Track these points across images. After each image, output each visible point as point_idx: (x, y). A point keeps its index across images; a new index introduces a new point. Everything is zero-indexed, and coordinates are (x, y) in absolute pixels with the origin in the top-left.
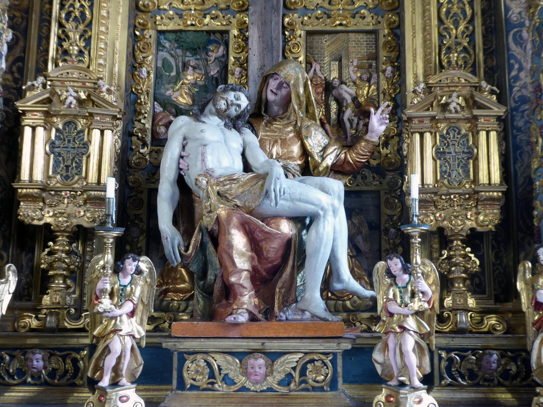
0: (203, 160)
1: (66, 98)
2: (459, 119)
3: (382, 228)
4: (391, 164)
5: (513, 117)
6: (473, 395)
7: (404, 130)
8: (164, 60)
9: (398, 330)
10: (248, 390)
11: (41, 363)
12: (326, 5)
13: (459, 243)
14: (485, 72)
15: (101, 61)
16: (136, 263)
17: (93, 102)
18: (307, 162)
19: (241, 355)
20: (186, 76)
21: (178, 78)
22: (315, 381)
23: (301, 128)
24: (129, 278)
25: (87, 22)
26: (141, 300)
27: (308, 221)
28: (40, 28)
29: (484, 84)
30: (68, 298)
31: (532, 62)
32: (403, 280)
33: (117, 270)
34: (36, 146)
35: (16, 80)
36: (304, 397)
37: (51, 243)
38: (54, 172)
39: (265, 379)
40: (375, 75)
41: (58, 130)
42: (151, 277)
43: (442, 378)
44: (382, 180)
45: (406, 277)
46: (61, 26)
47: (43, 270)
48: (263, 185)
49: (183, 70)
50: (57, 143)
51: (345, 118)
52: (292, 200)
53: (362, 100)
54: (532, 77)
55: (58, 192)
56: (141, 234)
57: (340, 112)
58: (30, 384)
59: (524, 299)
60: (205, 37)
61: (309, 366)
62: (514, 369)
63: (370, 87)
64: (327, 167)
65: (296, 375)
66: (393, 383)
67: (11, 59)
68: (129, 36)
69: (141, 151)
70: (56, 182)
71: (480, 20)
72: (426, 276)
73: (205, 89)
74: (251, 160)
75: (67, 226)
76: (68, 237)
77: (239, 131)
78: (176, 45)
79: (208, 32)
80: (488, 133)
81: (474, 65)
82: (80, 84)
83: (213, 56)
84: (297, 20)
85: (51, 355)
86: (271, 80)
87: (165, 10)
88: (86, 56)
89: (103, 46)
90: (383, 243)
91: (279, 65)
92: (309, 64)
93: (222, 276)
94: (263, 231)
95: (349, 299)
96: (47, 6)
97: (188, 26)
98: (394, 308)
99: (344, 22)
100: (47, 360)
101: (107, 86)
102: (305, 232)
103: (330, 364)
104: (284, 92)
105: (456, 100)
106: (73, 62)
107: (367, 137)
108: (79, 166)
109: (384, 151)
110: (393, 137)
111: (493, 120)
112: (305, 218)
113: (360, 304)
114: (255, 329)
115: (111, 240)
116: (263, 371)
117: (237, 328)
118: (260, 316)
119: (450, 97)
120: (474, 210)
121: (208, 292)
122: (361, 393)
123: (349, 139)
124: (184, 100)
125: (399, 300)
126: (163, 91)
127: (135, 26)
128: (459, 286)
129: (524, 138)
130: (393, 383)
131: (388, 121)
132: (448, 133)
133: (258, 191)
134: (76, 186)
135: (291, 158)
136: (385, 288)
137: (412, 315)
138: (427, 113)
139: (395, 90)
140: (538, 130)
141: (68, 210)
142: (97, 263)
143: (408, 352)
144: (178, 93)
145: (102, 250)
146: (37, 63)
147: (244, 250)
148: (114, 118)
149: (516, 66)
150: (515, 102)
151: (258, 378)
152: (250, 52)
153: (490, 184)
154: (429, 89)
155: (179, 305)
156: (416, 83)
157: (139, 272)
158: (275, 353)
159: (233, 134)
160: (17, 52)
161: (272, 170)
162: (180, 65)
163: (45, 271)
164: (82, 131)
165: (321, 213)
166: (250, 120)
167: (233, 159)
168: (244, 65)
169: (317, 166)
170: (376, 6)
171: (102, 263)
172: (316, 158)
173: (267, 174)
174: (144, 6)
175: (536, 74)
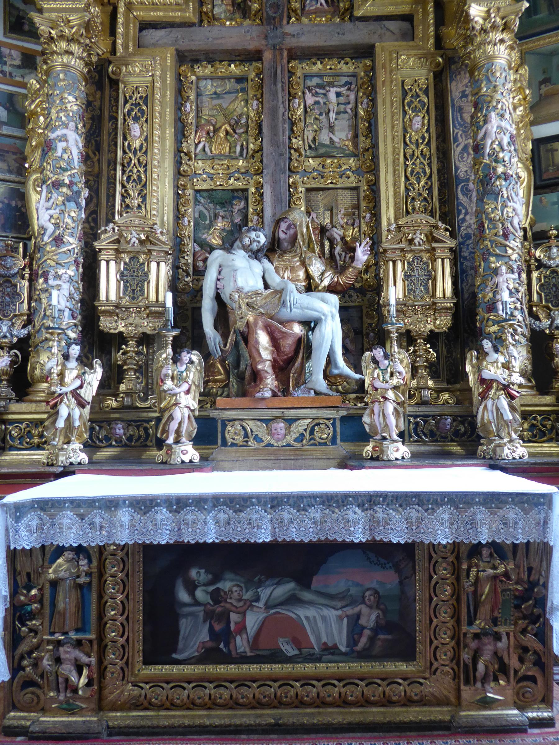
0: (235, 281)
1: (130, 240)
2: (421, 251)
3: (364, 333)
4: (370, 286)
5: (460, 249)
6: (433, 448)
7: (381, 259)
8: (200, 212)
9: (382, 400)
10: (273, 446)
11: (122, 431)
12: (320, 168)
13: (422, 341)
14: (440, 216)
15: (154, 212)
16: (189, 355)
17: (151, 242)
18: (309, 284)
19: (267, 421)
20: (217, 223)
21: (211, 225)
22: (320, 438)
23: (305, 258)
24: (185, 366)
25: (143, 183)
26: (193, 382)
27: (312, 325)
28: (108, 189)
29: (440, 223)
30: (138, 386)
31: (477, 206)
32: (384, 364)
33: (176, 360)
34: (110, 275)
35: (92, 228)
36: (313, 450)
37: (124, 347)
38: (124, 294)
39: (285, 438)
40: (357, 221)
41: (125, 263)
42: (200, 366)
43: (410, 436)
44: (364, 298)
45: (386, 362)
46: (123, 186)
47: (119, 365)
48: (280, 298)
49: (215, 219)
50: (125, 272)
51: (336, 252)
52: (302, 308)
53: (348, 239)
54: (477, 217)
55: (127, 308)
56: (188, 340)
57: (332, 248)
58: (114, 446)
59: (471, 378)
60: (230, 194)
61: (316, 428)
62: (462, 429)
63: (354, 229)
64: (325, 287)
65: (307, 434)
66: (378, 437)
67: (88, 212)
68: (174, 194)
69: (186, 279)
70: (126, 301)
71: (436, 177)
72: (401, 362)
73: (231, 232)
74: (269, 282)
75: (136, 334)
76: (136, 341)
77: (259, 260)
78: (209, 201)
79: (233, 191)
80: (443, 260)
81: (432, 211)
82: (140, 229)
83: (236, 208)
84: (299, 180)
85: (129, 425)
86: (282, 223)
87: (200, 174)
88: (144, 209)
89: (155, 201)
90: (365, 344)
91: (288, 212)
92: (308, 213)
93: (251, 365)
94: (281, 332)
95: (341, 385)
96: (113, 172)
97: (218, 186)
98: (378, 384)
99: (334, 181)
100: (126, 429)
101: (160, 230)
102: (310, 333)
103: (331, 426)
104: (292, 231)
105: (419, 236)
106: (135, 212)
107: (354, 265)
108: (142, 290)
109: (365, 277)
110: (371, 266)
111: (446, 251)
112: (311, 322)
113: (349, 388)
114: (277, 402)
115: (171, 338)
116: (283, 431)
117: (264, 401)
118: (279, 394)
119: (415, 234)
120: (433, 317)
121: (241, 377)
122: (353, 448)
123: (339, 268)
124: (216, 241)
125: (381, 379)
126: (200, 235)
127: (178, 187)
128: (422, 372)
129: (469, 265)
130: (378, 437)
131: (369, 253)
132: (413, 261)
133: (277, 302)
134: (140, 304)
135: (298, 280)
136: (371, 371)
137: (391, 389)
138: (398, 246)
139: (372, 231)
140: (481, 257)
141: (136, 322)
142: (161, 356)
143: (389, 414)
144: (211, 236)
145: (164, 346)
146: (107, 214)
147: (267, 345)
148: (167, 253)
149: (463, 211)
150: (462, 238)
151: (280, 437)
152: (265, 203)
153: (444, 297)
154: (399, 228)
155: (217, 391)
156: (389, 224)
157: (191, 362)
158: (291, 419)
159: (255, 263)
160: (92, 206)
161: (286, 286)
162: (212, 215)
163: (120, 367)
164: (143, 264)
165: (323, 318)
166: (267, 254)
167: (256, 280)
168: (260, 214)
169: (317, 286)
170: (358, 169)
171: (164, 356)
172: (317, 280)
173: (283, 290)
174: (184, 171)
175: (480, 215)
